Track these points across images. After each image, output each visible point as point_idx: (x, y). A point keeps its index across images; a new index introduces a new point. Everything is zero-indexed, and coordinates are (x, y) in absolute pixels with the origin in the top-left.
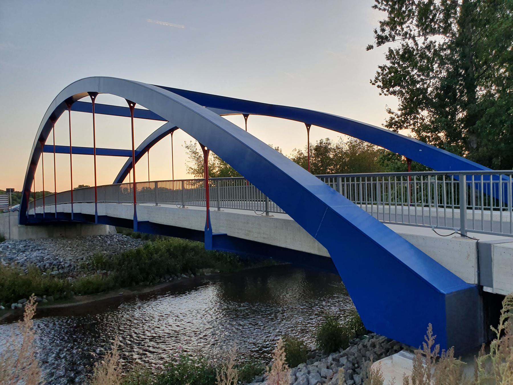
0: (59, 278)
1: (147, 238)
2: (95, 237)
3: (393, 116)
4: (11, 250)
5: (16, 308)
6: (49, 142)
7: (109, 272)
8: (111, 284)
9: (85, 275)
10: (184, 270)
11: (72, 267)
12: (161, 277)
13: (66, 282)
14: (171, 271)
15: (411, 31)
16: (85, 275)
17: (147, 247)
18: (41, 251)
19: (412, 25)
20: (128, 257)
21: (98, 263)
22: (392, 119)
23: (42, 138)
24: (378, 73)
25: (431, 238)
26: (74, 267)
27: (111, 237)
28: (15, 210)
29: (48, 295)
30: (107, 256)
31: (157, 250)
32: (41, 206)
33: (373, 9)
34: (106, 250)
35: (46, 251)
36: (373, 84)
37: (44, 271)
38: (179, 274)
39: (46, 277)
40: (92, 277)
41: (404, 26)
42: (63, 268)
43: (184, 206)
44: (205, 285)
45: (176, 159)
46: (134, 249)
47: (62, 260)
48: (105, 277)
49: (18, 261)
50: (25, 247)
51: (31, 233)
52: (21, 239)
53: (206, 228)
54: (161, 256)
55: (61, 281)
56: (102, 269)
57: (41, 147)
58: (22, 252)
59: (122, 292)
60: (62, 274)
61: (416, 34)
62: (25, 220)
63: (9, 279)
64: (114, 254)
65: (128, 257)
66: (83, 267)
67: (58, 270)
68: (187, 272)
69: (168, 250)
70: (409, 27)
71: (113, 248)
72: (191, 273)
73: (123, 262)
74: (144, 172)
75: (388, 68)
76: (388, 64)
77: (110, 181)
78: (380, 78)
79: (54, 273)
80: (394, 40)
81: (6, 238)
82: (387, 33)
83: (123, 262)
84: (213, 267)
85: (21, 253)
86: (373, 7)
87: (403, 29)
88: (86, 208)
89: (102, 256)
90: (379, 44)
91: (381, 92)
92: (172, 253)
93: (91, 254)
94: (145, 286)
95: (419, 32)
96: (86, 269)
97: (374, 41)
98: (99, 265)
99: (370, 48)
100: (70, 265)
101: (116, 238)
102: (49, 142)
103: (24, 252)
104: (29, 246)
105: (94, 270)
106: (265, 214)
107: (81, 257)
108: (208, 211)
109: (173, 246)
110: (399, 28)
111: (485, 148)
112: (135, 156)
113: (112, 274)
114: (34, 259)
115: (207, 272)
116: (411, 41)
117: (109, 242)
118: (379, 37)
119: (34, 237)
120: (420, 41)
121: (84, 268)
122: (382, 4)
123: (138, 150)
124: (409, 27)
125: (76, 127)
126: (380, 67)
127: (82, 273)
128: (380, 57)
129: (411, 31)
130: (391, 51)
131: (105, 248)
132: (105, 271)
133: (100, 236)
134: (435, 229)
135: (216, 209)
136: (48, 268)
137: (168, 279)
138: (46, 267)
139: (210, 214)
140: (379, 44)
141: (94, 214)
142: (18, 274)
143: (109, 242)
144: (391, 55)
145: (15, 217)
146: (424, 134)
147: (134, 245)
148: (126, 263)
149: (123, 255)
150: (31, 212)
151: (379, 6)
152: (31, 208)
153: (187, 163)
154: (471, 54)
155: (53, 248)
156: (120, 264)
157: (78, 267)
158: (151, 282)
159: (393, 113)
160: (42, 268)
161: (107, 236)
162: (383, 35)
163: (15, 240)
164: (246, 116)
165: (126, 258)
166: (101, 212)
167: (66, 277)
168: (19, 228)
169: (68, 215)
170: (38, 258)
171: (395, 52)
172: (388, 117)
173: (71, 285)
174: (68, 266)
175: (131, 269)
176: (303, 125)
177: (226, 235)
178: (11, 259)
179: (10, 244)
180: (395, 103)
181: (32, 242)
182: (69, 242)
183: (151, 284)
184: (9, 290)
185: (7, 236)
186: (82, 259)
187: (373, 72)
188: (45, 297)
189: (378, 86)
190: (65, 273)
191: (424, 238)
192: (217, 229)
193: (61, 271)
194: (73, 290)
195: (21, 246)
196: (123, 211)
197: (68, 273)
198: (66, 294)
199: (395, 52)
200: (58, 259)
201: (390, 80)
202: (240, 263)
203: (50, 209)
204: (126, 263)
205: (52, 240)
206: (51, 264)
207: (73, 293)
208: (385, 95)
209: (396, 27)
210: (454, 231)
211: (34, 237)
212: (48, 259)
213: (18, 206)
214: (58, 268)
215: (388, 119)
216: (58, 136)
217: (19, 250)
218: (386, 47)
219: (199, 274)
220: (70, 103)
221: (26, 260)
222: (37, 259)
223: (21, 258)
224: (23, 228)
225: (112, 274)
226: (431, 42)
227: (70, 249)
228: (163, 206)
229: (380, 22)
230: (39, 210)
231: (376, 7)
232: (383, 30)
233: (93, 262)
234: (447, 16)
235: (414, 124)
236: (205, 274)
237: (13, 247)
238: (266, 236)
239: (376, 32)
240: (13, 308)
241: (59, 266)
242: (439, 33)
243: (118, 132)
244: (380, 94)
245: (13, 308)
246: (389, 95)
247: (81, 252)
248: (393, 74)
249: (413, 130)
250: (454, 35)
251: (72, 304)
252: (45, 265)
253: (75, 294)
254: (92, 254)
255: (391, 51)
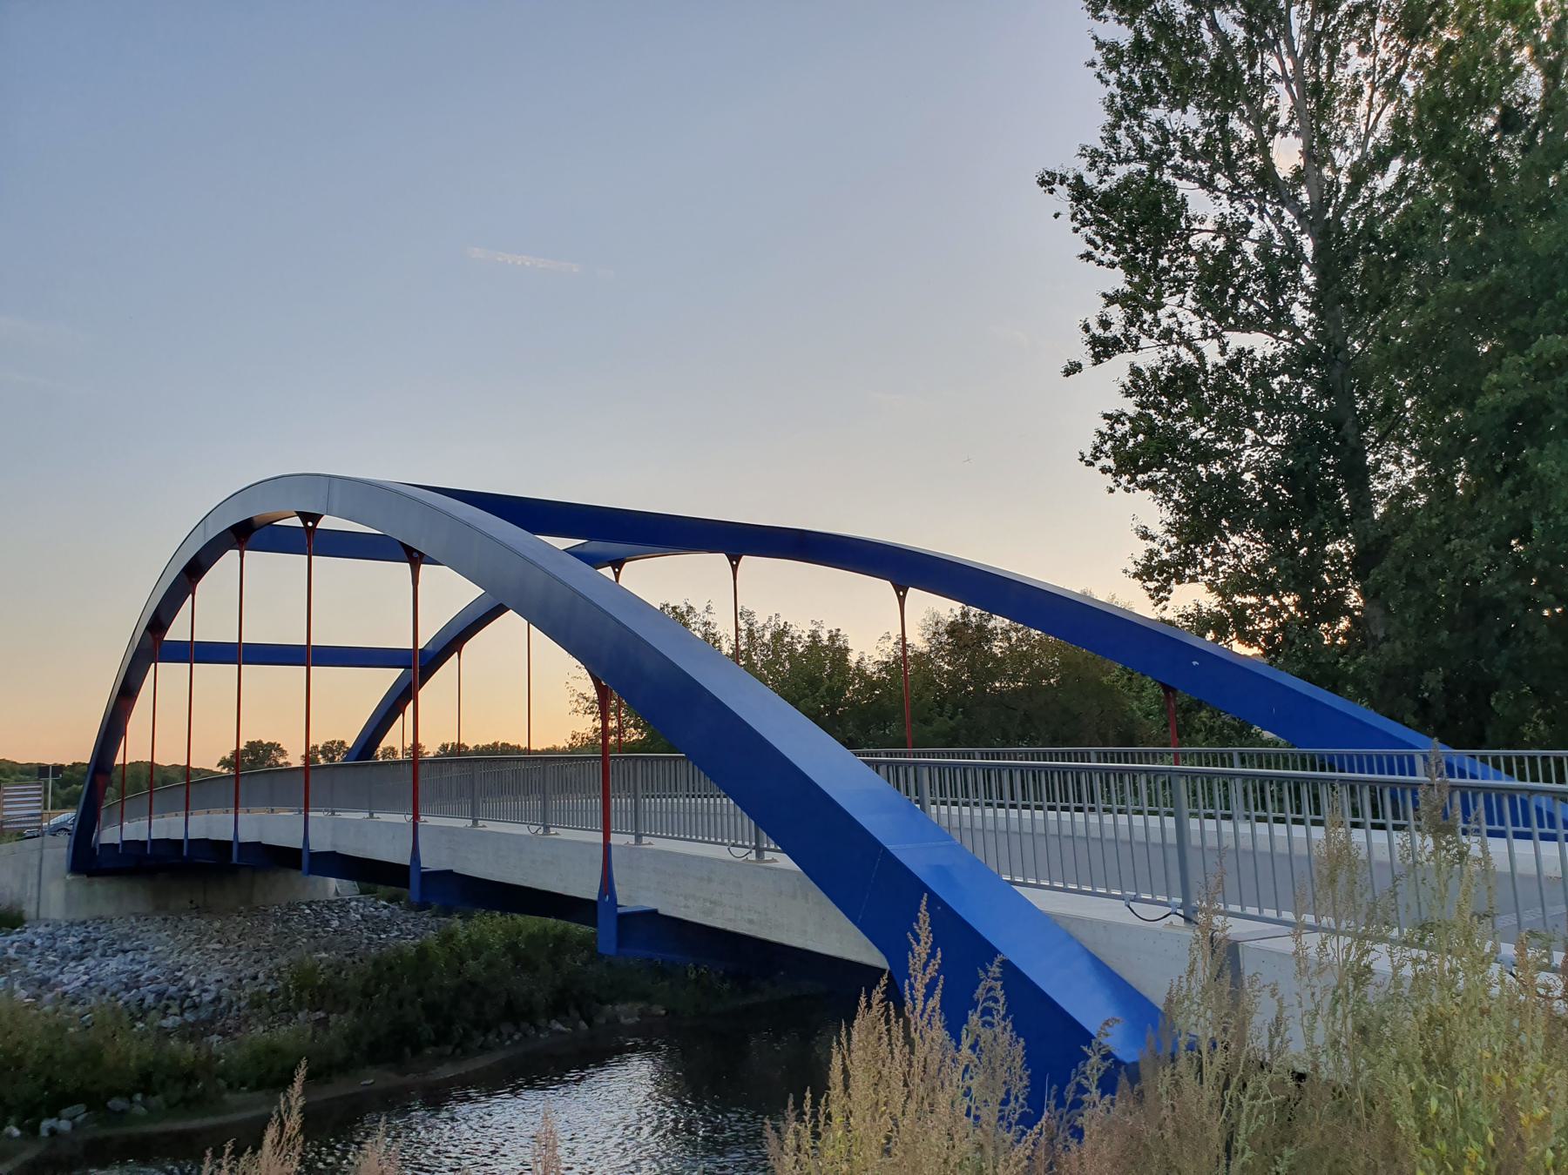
0: (183, 1039)
1: (448, 912)
2: (293, 907)
3: (1155, 546)
4: (42, 954)
5: (53, 1132)
6: (177, 631)
7: (333, 1018)
8: (340, 1055)
9: (261, 1028)
10: (558, 1009)
11: (224, 1004)
12: (487, 1030)
13: (204, 1050)
14: (517, 1013)
15: (1181, 325)
16: (261, 1028)
17: (447, 938)
18: (130, 955)
19: (1180, 310)
20: (390, 968)
21: (300, 988)
22: (1152, 554)
23: (158, 622)
24: (1101, 434)
25: (1120, 926)
26: (231, 1004)
27: (344, 905)
28: (57, 830)
29: (146, 1092)
30: (329, 966)
31: (477, 948)
32: (138, 816)
33: (1083, 262)
34: (326, 950)
35: (147, 956)
36: (1090, 464)
37: (140, 1019)
38: (542, 1022)
39: (143, 1036)
40: (283, 1034)
41: (1161, 313)
42: (195, 1006)
43: (547, 828)
44: (589, 1054)
45: (524, 691)
46: (409, 944)
47: (193, 982)
48: (320, 1032)
49: (65, 988)
50: (82, 942)
51: (106, 899)
52: (71, 917)
53: (602, 893)
54: (490, 965)
55: (191, 1047)
56: (314, 1008)
57: (153, 645)
58: (73, 959)
59: (370, 1079)
60: (192, 1025)
61: (1196, 331)
62: (87, 860)
63: (36, 1045)
64: (349, 960)
65: (390, 968)
66: (256, 1003)
67: (182, 1014)
68: (568, 1014)
69: (511, 947)
70: (1174, 315)
71: (347, 941)
72: (577, 1015)
73: (377, 985)
74: (444, 717)
75: (1131, 420)
76: (1130, 407)
77: (350, 735)
78: (1107, 447)
79: (169, 1022)
80: (1136, 349)
81: (26, 916)
82: (1117, 330)
83: (377, 985)
84: (645, 997)
85: (72, 964)
86: (1082, 257)
87: (1157, 322)
88: (275, 826)
89: (314, 968)
90: (1098, 359)
91: (1113, 485)
92: (520, 955)
93: (282, 960)
94: (440, 1059)
95: (1204, 326)
96: (265, 1009)
97: (1084, 354)
98: (306, 996)
99: (1073, 369)
100: (218, 999)
101: (356, 911)
102: (177, 631)
103: (80, 958)
104: (96, 940)
105: (288, 1010)
106: (753, 857)
107: (251, 971)
108: (607, 847)
109: (525, 933)
110: (1147, 316)
111: (1398, 644)
112: (419, 665)
113: (342, 1022)
114: (110, 981)
115: (627, 1013)
116: (1183, 351)
117: (335, 923)
118: (1095, 341)
119: (108, 910)
120: (1211, 349)
121: (259, 1006)
122: (1106, 249)
123: (430, 648)
124: (1174, 315)
125: (259, 595)
126: (1106, 416)
127: (253, 1020)
128: (1106, 390)
129: (1181, 325)
130: (1136, 372)
131: (323, 942)
132: (321, 1014)
133: (309, 906)
134: (1132, 905)
135: (631, 839)
136: (151, 1008)
137: (510, 1036)
138: (145, 1006)
139: (614, 852)
140: (1098, 359)
141: (300, 846)
142: (61, 1028)
143: (335, 923)
144: (1137, 383)
145: (59, 850)
146: (1237, 599)
147: (411, 931)
148: (386, 987)
149: (376, 963)
150: (109, 835)
151: (1098, 254)
152: (109, 823)
153: (573, 683)
154: (1347, 386)
155: (166, 944)
156: (367, 994)
157: (243, 1004)
158: (458, 1046)
159: (1153, 539)
160: (133, 1007)
161: (329, 905)
162: (1108, 334)
163: (55, 921)
164: (734, 559)
165: (386, 970)
166: (321, 842)
167: (203, 1035)
168: (68, 884)
169: (223, 847)
170: (124, 978)
171: (1148, 374)
172: (1140, 549)
173: (219, 1058)
174: (212, 1002)
175: (400, 1006)
176: (885, 587)
177: (655, 912)
178: (44, 982)
179: (39, 935)
180: (1148, 513)
181: (103, 928)
182: (217, 925)
183: (459, 1051)
184: (35, 1078)
185: (30, 910)
186: (255, 978)
187: (1087, 430)
188: (138, 1097)
189: (1104, 470)
190: (203, 1022)
191: (1106, 925)
192: (634, 895)
193: (190, 1017)
194: (223, 1074)
195: (72, 939)
196: (380, 833)
197: (212, 1021)
198: (204, 1089)
199: (1148, 374)
200: (181, 978)
201: (1136, 454)
202: (727, 986)
203: (168, 826)
204: (386, 987)
205: (165, 920)
206: (160, 995)
207: (222, 1083)
208: (1127, 490)
209: (1141, 315)
210: (1169, 910)
211: (108, 910)
212: (153, 980)
213: (68, 816)
214: (181, 1006)
215: (1140, 555)
216: (209, 615)
217: (65, 955)
218: (1119, 366)
219: (602, 1021)
220: (246, 534)
221: (85, 985)
222: (120, 982)
223: (72, 978)
224: (79, 884)
225: (342, 1022)
226: (1241, 351)
227: (218, 946)
228: (492, 826)
229: (1105, 295)
230: (135, 830)
231: (1088, 256)
232: (1105, 324)
233: (286, 987)
234: (1275, 288)
235: (1214, 569)
236: (623, 1020)
237: (47, 944)
238: (755, 917)
239: (1087, 328)
240: (44, 1133)
241: (185, 1002)
242: (1260, 328)
243: (371, 602)
244: (1111, 491)
245: (44, 1133)
246: (1138, 491)
247: (249, 954)
248: (1141, 437)
249: (1211, 586)
250: (1297, 332)
251: (220, 1120)
252: (143, 1000)
253: (230, 1086)
254: (285, 962)
255: (1136, 372)
